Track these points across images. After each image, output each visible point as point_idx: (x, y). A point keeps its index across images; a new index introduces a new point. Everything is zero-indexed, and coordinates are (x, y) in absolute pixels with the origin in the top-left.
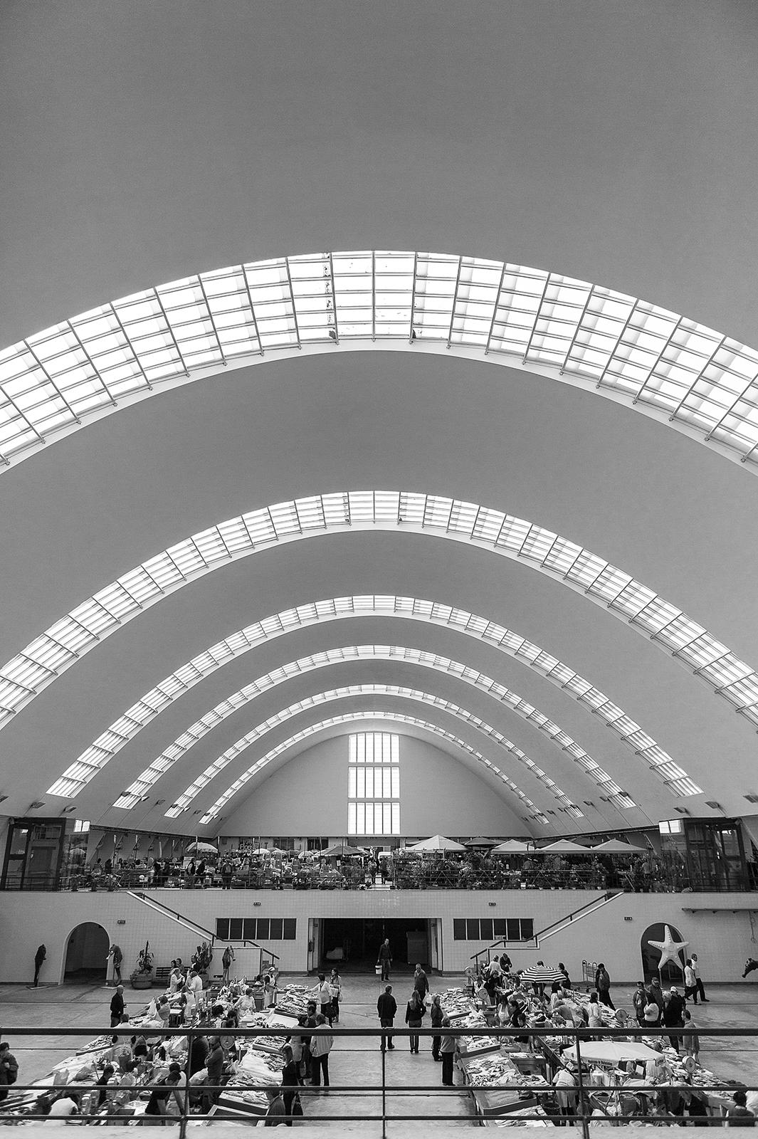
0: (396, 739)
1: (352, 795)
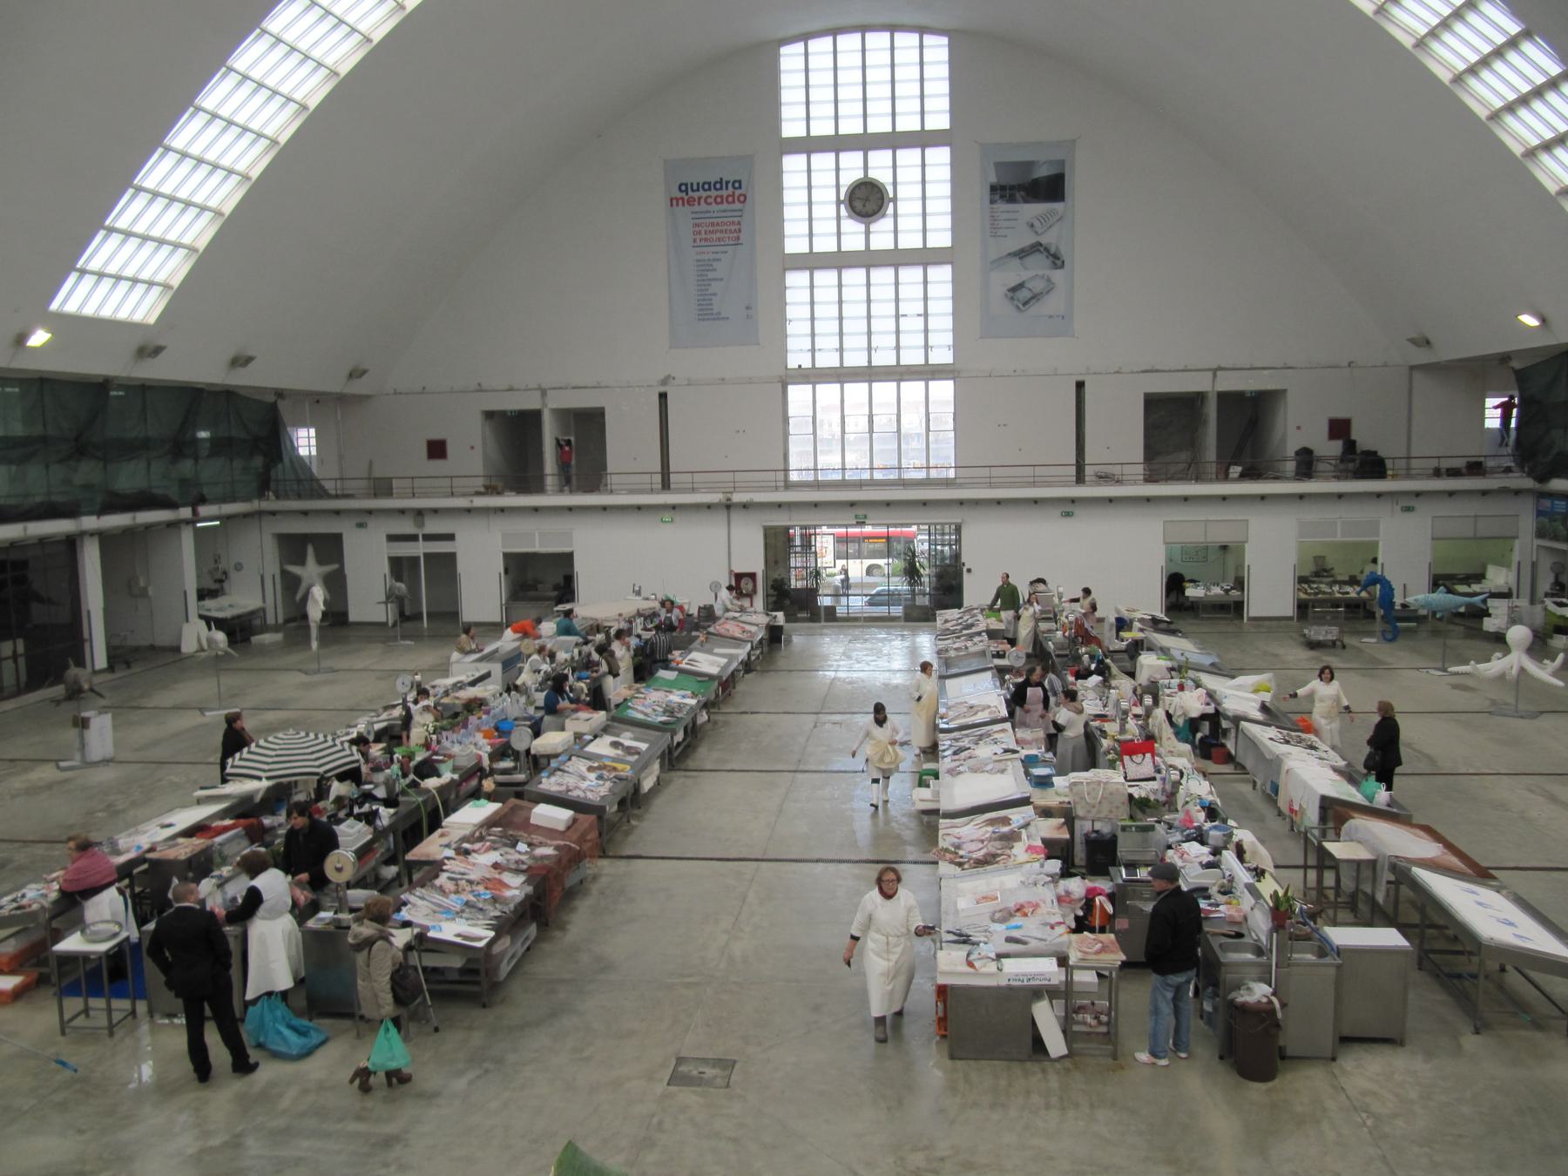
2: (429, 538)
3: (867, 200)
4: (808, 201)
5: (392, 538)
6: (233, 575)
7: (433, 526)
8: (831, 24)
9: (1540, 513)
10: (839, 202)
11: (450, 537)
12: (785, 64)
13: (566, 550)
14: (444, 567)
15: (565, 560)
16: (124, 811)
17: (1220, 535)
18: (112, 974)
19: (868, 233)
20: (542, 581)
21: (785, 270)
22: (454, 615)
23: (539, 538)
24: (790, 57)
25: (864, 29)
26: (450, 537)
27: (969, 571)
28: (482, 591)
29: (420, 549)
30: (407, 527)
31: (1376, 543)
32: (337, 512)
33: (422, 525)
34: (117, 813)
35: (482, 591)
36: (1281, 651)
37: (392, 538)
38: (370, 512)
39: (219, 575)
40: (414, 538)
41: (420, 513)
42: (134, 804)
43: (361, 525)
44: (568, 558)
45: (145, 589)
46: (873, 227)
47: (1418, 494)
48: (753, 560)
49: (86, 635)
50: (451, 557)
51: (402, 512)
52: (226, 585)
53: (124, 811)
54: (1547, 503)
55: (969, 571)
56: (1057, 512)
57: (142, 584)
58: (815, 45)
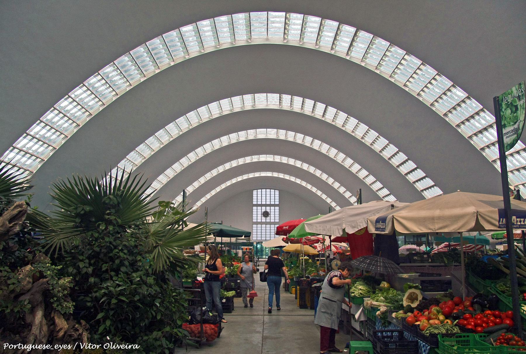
0: (277, 192)
1: (255, 203)
3: (266, 214)
4: (257, 214)
12: (254, 193)
24: (255, 192)
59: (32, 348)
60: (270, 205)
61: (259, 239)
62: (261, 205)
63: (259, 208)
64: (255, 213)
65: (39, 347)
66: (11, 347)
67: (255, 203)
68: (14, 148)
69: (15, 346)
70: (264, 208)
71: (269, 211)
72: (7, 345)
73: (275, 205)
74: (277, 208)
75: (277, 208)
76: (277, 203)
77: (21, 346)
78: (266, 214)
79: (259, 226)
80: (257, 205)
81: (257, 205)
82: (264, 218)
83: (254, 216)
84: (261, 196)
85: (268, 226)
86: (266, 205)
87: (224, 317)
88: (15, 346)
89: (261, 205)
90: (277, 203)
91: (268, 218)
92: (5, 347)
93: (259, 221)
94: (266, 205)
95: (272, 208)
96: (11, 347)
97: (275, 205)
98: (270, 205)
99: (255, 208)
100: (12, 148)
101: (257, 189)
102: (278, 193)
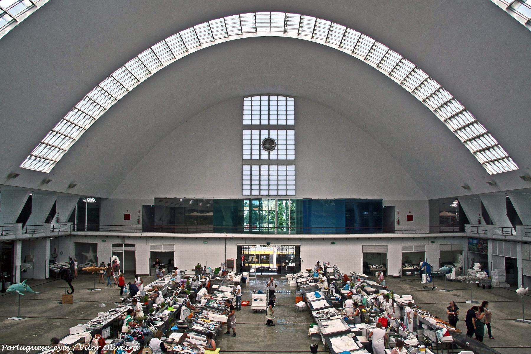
0: (291, 102)
1: (247, 122)
2: (126, 246)
3: (269, 144)
4: (251, 143)
5: (114, 245)
6: (59, 255)
7: (128, 242)
8: (261, 92)
9: (469, 243)
10: (260, 145)
11: (134, 246)
12: (245, 103)
13: (172, 251)
14: (130, 256)
15: (171, 255)
16: (43, 334)
17: (379, 250)
18: (297, 310)
19: (269, 154)
20: (163, 262)
21: (243, 164)
22: (133, 272)
23: (163, 248)
24: (247, 102)
25: (269, 95)
26: (133, 246)
27: (303, 261)
28: (143, 266)
29: (123, 249)
30: (118, 242)
31: (424, 253)
32: (96, 236)
33: (124, 242)
34: (41, 335)
35: (143, 266)
36: (401, 286)
37: (114, 245)
38: (107, 236)
39: (55, 256)
40: (121, 246)
41: (124, 237)
42: (46, 332)
43: (104, 241)
44: (172, 254)
45: (32, 259)
46: (271, 153)
47: (435, 238)
48: (233, 255)
49: (14, 274)
50: (134, 252)
51: (118, 237)
52: (57, 259)
53: (43, 334)
54: (471, 240)
55: (303, 261)
56: (330, 242)
57: (31, 257)
58: (254, 98)
59: (31, 350)
60: (278, 127)
61: (256, 193)
62: (260, 127)
63: (256, 132)
64: (246, 142)
65: (38, 349)
66: (9, 348)
67: (247, 122)
68: (32, 156)
69: (14, 348)
70: (265, 132)
71: (274, 138)
72: (5, 346)
73: (286, 127)
74: (291, 132)
75: (291, 132)
76: (291, 122)
77: (19, 348)
78: (269, 144)
79: (255, 167)
80: (251, 127)
81: (251, 127)
82: (264, 153)
83: (246, 147)
84: (257, 109)
85: (273, 167)
86: (269, 127)
87: (514, 8)
88: (14, 348)
89: (260, 127)
90: (291, 122)
91: (274, 152)
92: (3, 348)
93: (256, 157)
94: (269, 127)
95: (282, 132)
96: (9, 348)
97: (286, 127)
98: (278, 127)
99: (247, 132)
100: (29, 156)
101: (251, 96)
102: (293, 103)
